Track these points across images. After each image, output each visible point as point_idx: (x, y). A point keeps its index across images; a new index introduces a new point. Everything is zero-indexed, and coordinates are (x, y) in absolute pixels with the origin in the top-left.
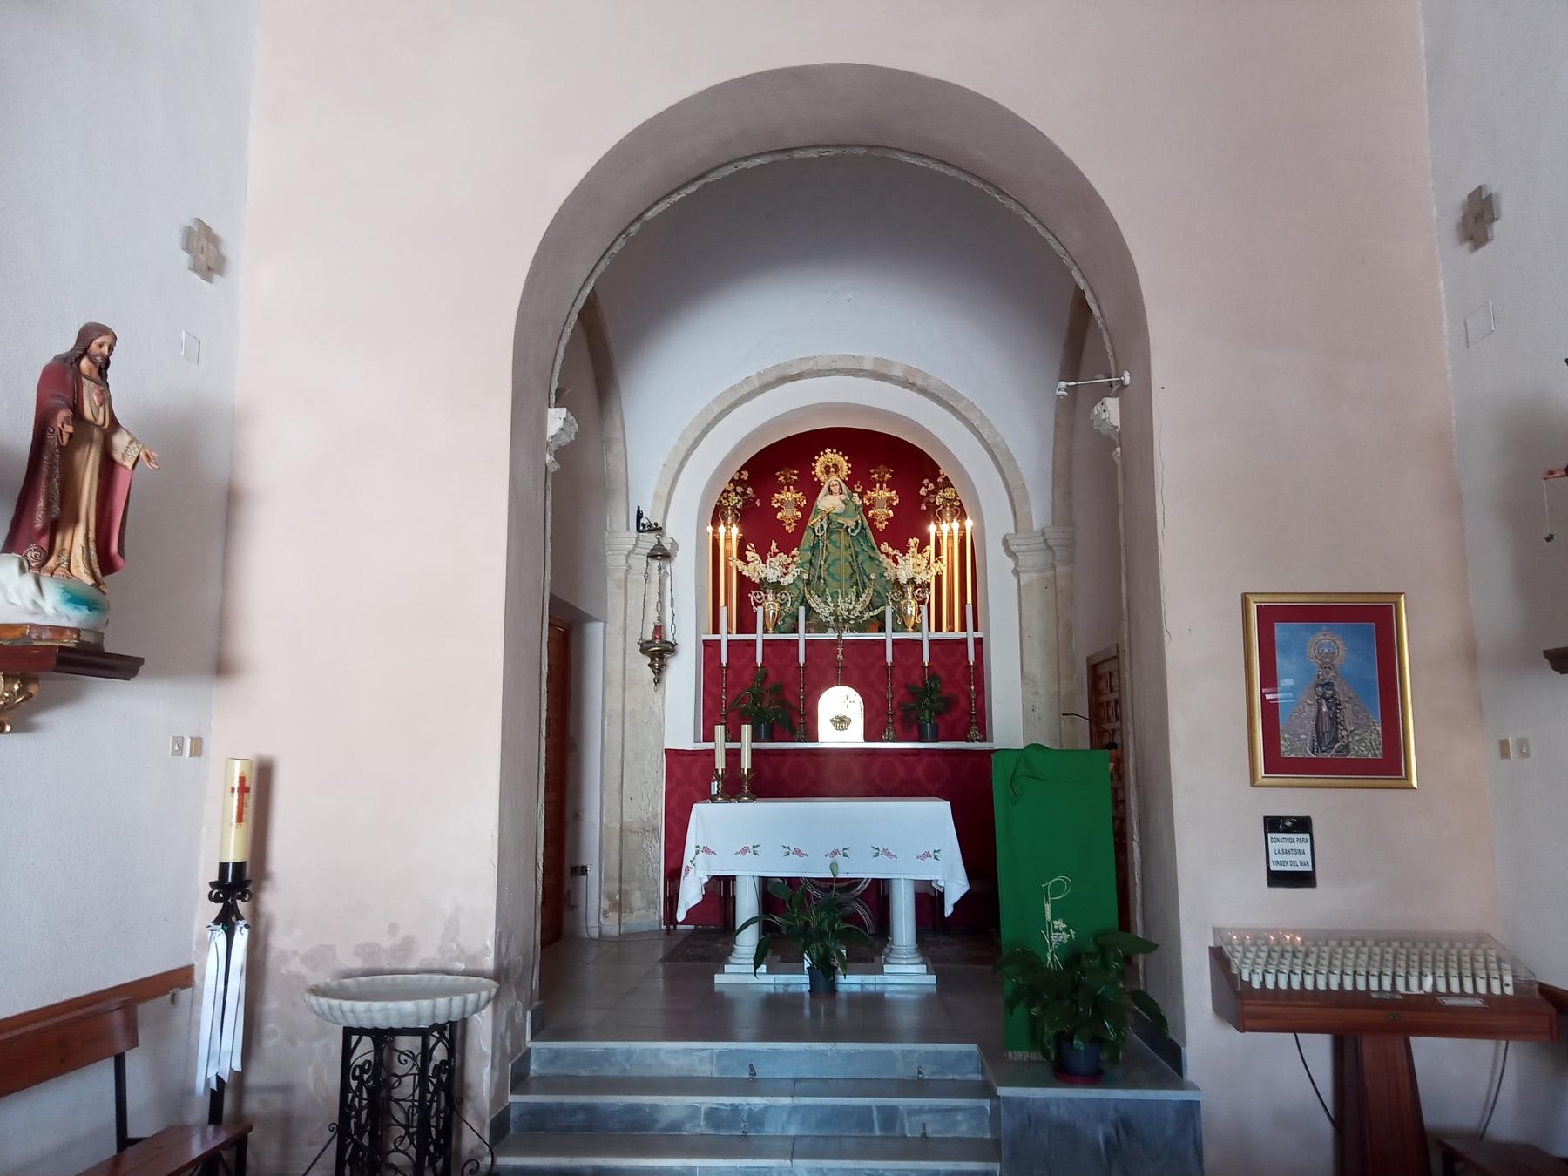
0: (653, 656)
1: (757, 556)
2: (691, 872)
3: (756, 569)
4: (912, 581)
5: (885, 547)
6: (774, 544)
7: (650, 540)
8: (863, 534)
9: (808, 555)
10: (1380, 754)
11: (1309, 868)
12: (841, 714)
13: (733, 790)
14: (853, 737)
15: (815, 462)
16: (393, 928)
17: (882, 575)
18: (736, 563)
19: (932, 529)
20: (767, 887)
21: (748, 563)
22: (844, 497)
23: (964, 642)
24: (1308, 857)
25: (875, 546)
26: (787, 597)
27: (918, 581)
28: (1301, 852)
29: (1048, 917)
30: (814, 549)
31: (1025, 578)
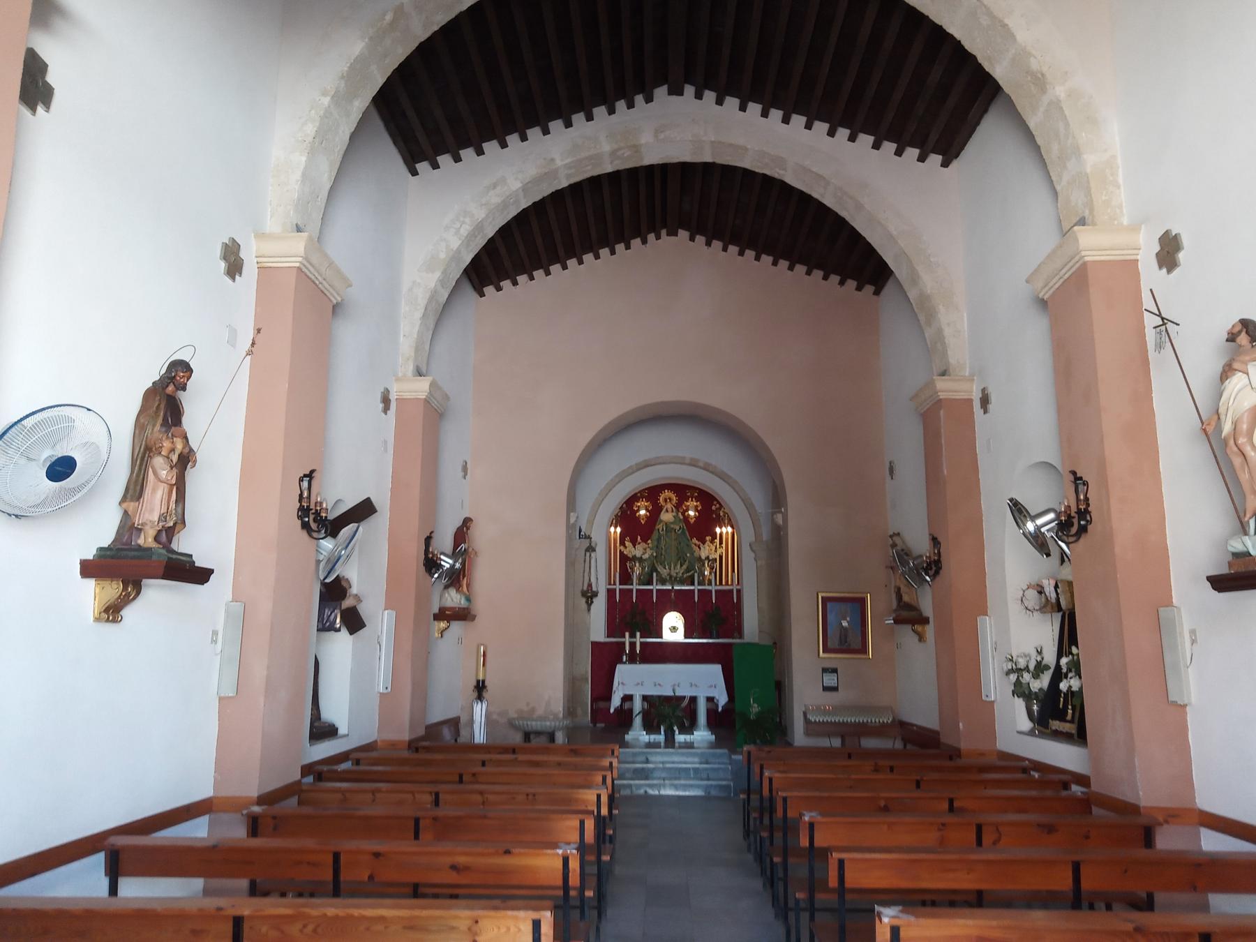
0: (588, 598)
1: (631, 544)
2: (616, 693)
3: (630, 550)
4: (707, 558)
5: (695, 540)
6: (639, 537)
7: (586, 543)
8: (683, 533)
9: (656, 543)
10: (860, 647)
13: (633, 659)
14: (679, 637)
15: (660, 496)
17: (693, 554)
19: (718, 530)
20: (645, 698)
22: (674, 514)
23: (731, 591)
25: (689, 538)
26: (646, 564)
27: (711, 558)
28: (834, 680)
30: (659, 540)
31: (759, 563)
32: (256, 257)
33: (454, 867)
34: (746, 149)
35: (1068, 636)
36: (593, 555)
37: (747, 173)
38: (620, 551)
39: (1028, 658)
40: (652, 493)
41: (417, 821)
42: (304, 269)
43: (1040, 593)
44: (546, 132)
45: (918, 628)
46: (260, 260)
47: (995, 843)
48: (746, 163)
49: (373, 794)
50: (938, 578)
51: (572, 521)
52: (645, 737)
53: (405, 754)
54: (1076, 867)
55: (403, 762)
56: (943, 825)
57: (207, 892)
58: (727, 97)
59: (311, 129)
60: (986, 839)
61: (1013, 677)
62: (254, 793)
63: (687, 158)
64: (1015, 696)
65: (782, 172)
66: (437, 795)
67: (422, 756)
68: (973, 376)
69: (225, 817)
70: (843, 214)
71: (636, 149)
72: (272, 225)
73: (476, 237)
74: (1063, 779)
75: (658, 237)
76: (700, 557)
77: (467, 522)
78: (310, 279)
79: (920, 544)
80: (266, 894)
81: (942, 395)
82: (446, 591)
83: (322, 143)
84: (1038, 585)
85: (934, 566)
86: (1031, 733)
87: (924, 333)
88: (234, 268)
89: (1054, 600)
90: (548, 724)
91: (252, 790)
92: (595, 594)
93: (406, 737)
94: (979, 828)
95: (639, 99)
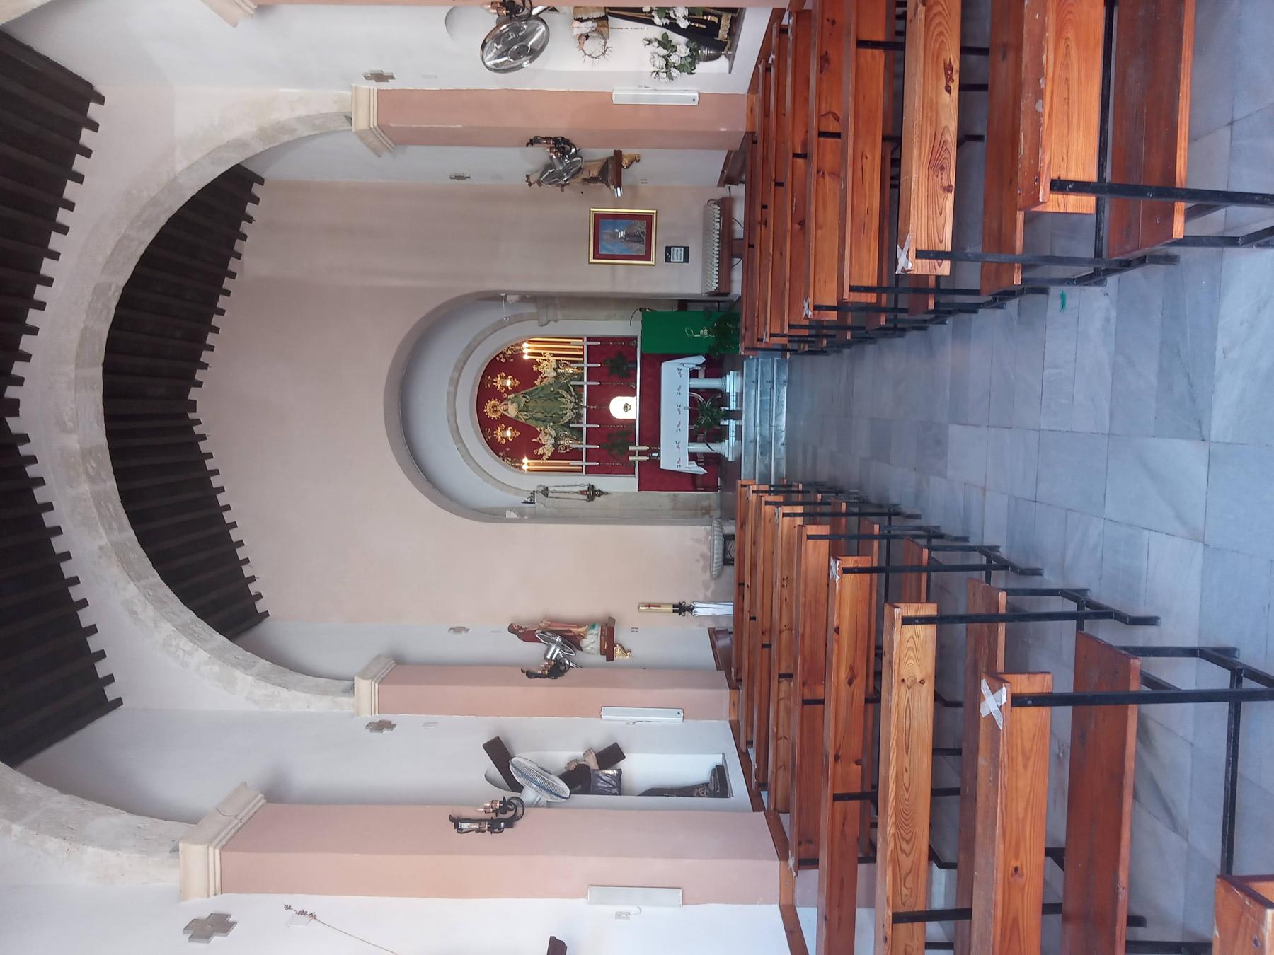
0: (594, 495)
1: (541, 449)
3: (547, 449)
4: (555, 370)
5: (537, 382)
7: (539, 497)
8: (529, 394)
9: (539, 422)
11: (683, 249)
12: (623, 407)
14: (634, 402)
15: (491, 417)
16: (697, 561)
17: (551, 385)
18: (544, 460)
19: (526, 357)
20: (693, 439)
21: (544, 453)
22: (509, 403)
24: (679, 249)
25: (536, 387)
26: (562, 433)
28: (677, 251)
29: (699, 336)
30: (537, 419)
32: (209, 896)
33: (850, 683)
34: (86, 328)
35: (637, 15)
36: (551, 489)
37: (116, 326)
38: (548, 459)
39: (656, 56)
40: (486, 425)
41: (805, 702)
42: (223, 843)
43: (587, 37)
44: (67, 556)
45: (625, 161)
46: (212, 891)
47: (838, 119)
48: (104, 329)
49: (779, 739)
50: (573, 142)
51: (514, 515)
52: (731, 441)
53: (743, 692)
54: (862, 44)
55: (750, 698)
56: (818, 172)
57: (870, 904)
58: (20, 348)
59: (53, 844)
60: (832, 126)
61: (675, 72)
62: (776, 864)
63: (98, 394)
64: (693, 72)
65: (113, 288)
66: (780, 676)
67: (744, 676)
68: (351, 86)
69: (799, 891)
70: (163, 220)
71: (87, 454)
72: (170, 879)
73: (194, 631)
74: (776, 31)
75: (198, 422)
76: (554, 377)
77: (512, 629)
78: (235, 834)
79: (541, 154)
80: (873, 847)
81: (374, 123)
82: (583, 649)
83: (72, 829)
84: (579, 39)
85: (561, 145)
86: (731, 59)
87: (305, 137)
88: (220, 924)
89: (595, 25)
90: (718, 544)
91: (773, 866)
92: (591, 487)
93: (726, 692)
94: (822, 134)
95: (24, 450)
